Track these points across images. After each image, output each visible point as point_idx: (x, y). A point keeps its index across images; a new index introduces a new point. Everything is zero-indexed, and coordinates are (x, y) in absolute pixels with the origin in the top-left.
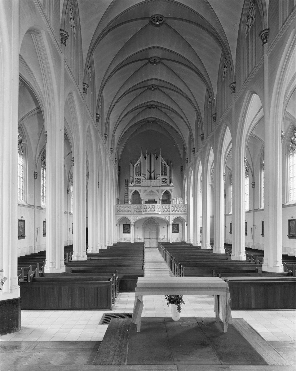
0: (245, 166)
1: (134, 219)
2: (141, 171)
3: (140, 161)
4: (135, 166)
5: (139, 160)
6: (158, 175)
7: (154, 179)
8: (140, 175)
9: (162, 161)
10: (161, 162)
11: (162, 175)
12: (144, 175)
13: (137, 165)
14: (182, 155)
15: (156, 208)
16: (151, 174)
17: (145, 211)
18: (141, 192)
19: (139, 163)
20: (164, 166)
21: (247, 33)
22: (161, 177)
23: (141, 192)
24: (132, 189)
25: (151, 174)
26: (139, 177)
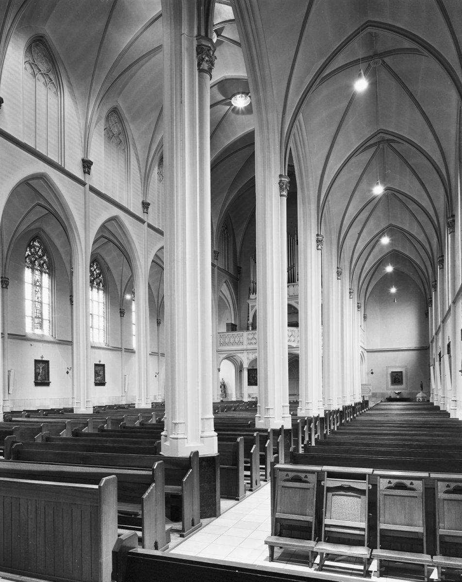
1: (248, 358)
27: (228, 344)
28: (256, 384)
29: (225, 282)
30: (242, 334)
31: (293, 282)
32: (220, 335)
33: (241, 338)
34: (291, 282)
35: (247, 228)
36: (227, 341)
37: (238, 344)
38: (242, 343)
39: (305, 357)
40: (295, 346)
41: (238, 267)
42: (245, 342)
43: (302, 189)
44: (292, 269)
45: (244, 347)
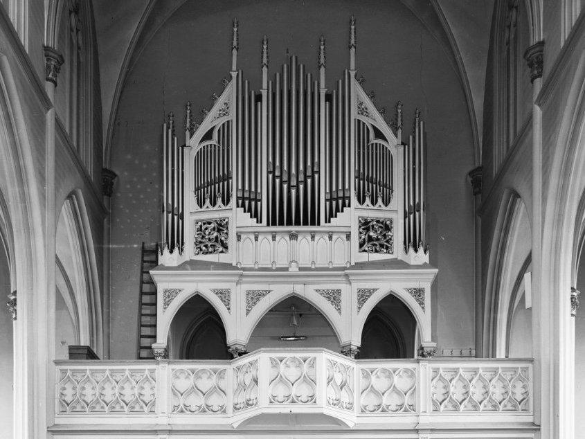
0: (572, 315)
2: (227, 177)
3: (224, 113)
4: (194, 144)
5: (219, 104)
6: (338, 203)
7: (315, 221)
8: (226, 201)
9: (363, 111)
10: (354, 115)
11: (361, 200)
12: (249, 204)
13: (208, 136)
14: (478, 103)
15: (322, 378)
16: (293, 191)
17: (248, 404)
18: (228, 305)
19: (219, 123)
20: (373, 140)
21: (508, 43)
22: (350, 217)
23: (228, 305)
24: (177, 282)
25: (293, 191)
26: (214, 213)
27: (92, 408)
28: (70, 358)
29: (69, 197)
30: (152, 371)
31: (313, 224)
32: (64, 372)
33: (147, 386)
34: (305, 223)
35: (140, 41)
36: (89, 394)
37: (133, 407)
38: (151, 406)
39: (93, 336)
40: (351, 426)
41: (105, 170)
42: (164, 401)
43: (16, 329)
44: (309, 181)
45: (162, 420)
